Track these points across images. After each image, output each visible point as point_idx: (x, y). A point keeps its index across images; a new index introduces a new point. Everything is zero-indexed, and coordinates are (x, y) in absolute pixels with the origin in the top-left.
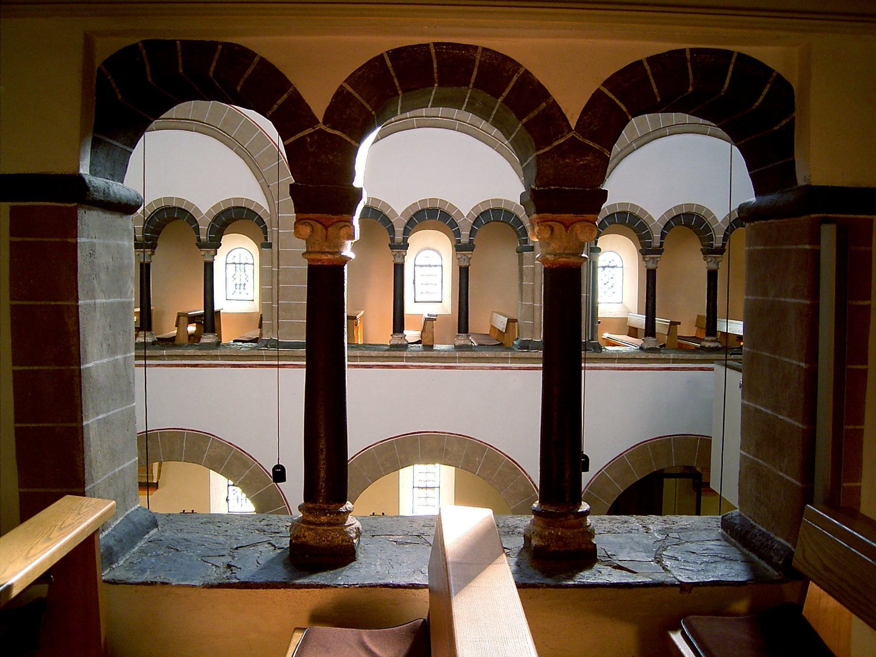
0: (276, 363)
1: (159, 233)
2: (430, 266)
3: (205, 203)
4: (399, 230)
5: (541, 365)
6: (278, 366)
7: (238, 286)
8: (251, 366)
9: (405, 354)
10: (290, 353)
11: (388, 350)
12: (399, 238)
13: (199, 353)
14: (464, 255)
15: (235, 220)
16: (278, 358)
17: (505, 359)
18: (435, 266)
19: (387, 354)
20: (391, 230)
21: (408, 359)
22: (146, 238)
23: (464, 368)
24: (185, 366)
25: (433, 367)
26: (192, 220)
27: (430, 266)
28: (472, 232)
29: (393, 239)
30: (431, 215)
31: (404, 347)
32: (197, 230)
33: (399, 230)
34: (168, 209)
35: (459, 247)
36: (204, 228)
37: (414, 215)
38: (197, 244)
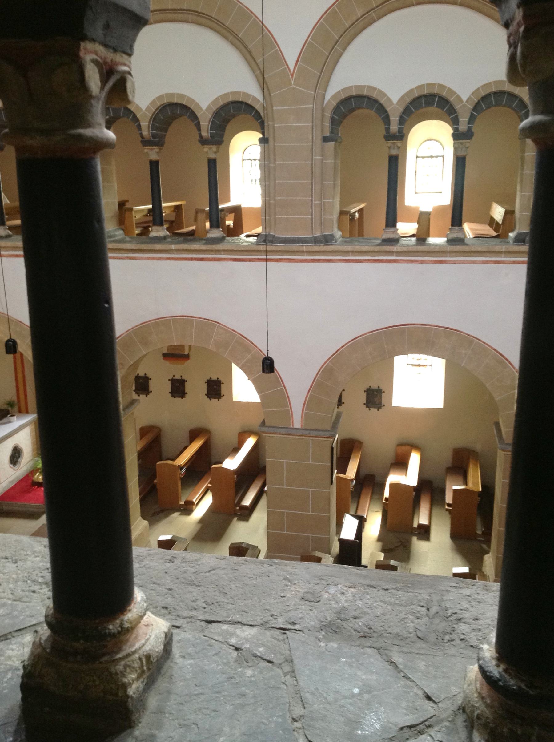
0: (264, 257)
1: (166, 130)
2: (432, 157)
3: (205, 98)
4: (394, 119)
5: (526, 259)
6: (266, 260)
7: (254, 181)
8: (250, 260)
9: (395, 248)
10: (286, 249)
11: (379, 245)
12: (394, 128)
13: (204, 247)
14: (462, 144)
15: (234, 116)
16: (266, 252)
17: (498, 253)
18: (437, 157)
19: (377, 248)
20: (387, 120)
21: (399, 253)
22: (154, 136)
23: (454, 262)
24: (192, 259)
25: (422, 262)
26: (193, 116)
27: (432, 157)
28: (472, 119)
29: (388, 130)
30: (430, 103)
31: (395, 241)
32: (139, 127)
33: (394, 119)
34: (185, 108)
35: (457, 136)
36: (205, 124)
37: (411, 103)
38: (199, 141)
